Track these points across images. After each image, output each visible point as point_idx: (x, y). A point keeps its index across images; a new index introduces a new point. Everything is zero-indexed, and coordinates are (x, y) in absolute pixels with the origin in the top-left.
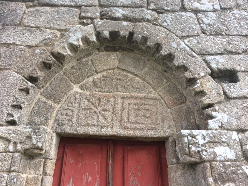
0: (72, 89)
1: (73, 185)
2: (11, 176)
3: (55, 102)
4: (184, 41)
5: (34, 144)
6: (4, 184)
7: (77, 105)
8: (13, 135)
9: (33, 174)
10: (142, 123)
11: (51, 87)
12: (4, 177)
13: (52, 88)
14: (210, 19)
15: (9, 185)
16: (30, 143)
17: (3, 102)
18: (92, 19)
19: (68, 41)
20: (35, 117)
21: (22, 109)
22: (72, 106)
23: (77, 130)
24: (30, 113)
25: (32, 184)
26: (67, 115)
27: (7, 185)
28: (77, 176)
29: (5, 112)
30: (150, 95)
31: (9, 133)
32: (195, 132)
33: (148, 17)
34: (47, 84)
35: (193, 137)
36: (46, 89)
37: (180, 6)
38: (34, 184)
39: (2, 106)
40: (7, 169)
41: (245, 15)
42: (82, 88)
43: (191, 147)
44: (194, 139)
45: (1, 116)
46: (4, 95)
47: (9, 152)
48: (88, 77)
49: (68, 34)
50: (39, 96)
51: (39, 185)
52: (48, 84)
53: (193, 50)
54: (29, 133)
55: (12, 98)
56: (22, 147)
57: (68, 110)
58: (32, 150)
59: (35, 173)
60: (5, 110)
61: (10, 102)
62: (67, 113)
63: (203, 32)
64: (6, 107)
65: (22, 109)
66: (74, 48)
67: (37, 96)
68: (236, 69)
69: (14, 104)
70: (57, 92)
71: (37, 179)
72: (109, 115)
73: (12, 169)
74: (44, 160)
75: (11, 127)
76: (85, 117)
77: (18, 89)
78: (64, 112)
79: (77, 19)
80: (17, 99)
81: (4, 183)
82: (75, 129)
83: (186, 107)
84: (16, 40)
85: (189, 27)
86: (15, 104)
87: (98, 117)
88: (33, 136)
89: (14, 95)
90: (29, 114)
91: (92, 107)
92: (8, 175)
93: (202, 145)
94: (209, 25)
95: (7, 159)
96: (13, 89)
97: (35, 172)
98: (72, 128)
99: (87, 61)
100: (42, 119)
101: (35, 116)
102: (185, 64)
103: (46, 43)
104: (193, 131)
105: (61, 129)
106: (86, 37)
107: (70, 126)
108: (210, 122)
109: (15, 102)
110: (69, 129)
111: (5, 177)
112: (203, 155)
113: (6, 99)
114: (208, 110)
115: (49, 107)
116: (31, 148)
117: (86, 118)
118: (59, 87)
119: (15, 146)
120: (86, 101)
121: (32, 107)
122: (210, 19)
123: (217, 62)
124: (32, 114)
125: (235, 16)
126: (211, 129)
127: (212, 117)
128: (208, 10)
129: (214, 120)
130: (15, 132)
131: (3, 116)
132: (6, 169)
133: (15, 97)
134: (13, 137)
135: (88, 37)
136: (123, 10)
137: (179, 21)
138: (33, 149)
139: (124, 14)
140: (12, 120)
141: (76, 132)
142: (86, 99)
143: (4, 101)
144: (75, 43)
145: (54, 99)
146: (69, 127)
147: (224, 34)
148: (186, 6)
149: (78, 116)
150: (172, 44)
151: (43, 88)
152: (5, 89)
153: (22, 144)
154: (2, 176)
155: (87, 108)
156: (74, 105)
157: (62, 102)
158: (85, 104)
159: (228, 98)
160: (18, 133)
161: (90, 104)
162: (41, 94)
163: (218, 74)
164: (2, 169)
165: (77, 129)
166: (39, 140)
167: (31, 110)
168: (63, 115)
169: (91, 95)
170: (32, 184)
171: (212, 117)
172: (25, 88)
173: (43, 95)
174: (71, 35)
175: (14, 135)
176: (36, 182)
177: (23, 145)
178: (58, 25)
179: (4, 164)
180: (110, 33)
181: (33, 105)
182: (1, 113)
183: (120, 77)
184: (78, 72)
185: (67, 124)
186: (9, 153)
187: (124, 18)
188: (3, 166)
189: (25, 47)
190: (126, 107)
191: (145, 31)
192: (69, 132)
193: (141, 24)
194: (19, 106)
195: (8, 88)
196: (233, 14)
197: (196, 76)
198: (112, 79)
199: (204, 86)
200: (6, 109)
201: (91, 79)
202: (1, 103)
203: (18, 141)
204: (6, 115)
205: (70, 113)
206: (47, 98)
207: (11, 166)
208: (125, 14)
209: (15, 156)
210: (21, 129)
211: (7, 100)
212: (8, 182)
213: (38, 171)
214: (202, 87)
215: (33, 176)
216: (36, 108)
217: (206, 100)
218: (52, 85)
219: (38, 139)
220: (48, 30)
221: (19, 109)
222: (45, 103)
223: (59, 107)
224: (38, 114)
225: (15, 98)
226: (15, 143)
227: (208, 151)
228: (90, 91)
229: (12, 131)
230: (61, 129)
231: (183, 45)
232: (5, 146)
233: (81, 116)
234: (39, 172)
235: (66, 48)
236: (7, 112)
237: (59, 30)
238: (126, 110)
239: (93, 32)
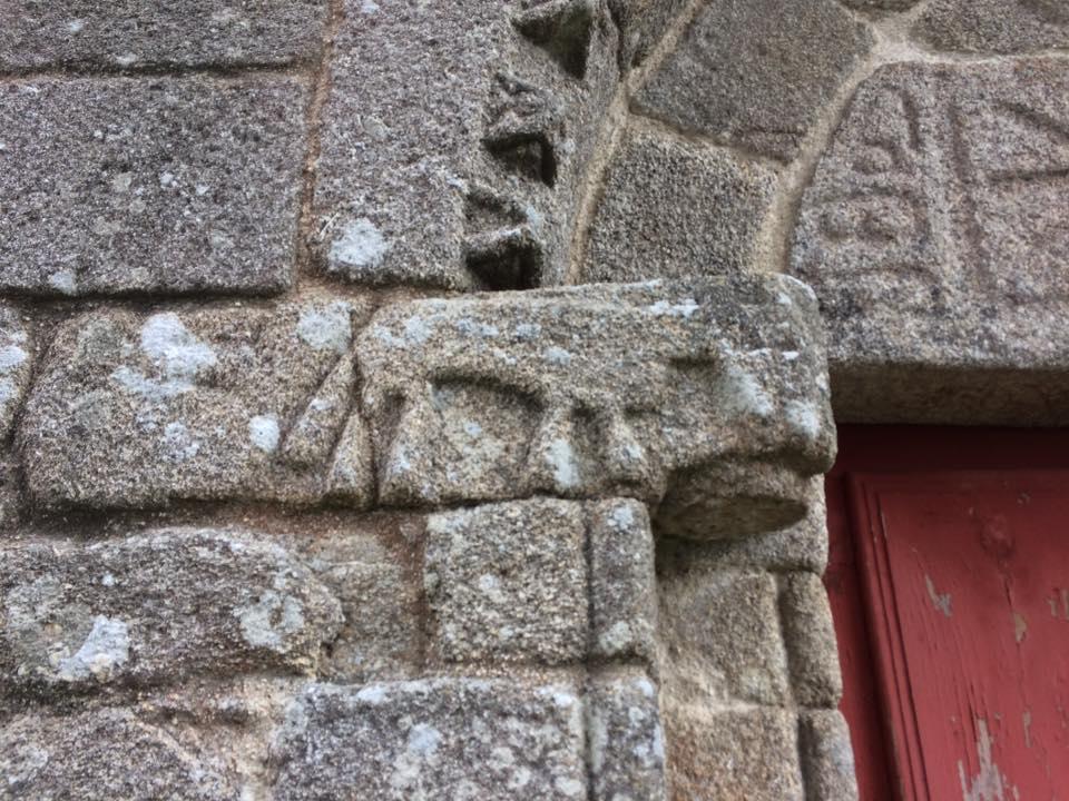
0: (865, 52)
1: (1007, 793)
2: (620, 704)
3: (752, 152)
5: (755, 416)
6: (573, 787)
7: (935, 153)
8: (556, 352)
9: (712, 692)
11: (698, 50)
12: (554, 714)
13: (706, 63)
15: (627, 788)
16: (710, 407)
17: (416, 122)
20: (627, 264)
21: (550, 184)
22: (898, 164)
23: (992, 337)
24: (578, 237)
25: (730, 785)
26: (873, 231)
27: (600, 787)
28: (1027, 719)
29: (452, 186)
31: (520, 339)
34: (664, 42)
36: (666, 68)
38: (745, 778)
39: (417, 150)
40: (566, 636)
45: (427, 215)
46: (417, 67)
47: (548, 490)
50: (623, 124)
51: (796, 790)
52: (670, 38)
54: (683, 326)
55: (485, 84)
56: (650, 450)
57: (876, 198)
58: (742, 471)
59: (734, 689)
60: (442, 172)
61: (474, 111)
62: (869, 217)
64: (452, 149)
65: (550, 184)
67: (609, 127)
69: (500, 125)
70: (753, 77)
71: (766, 741)
73: (617, 636)
74: (773, 584)
76: (1036, 235)
77: (514, 23)
78: (847, 214)
80: (520, 89)
81: (570, 776)
82: (971, 332)
86: (513, 130)
88: (729, 351)
89: (489, 67)
90: (579, 245)
92: (582, 692)
95: (549, 555)
96: (478, 23)
97: (732, 678)
98: (945, 327)
100: (687, 271)
101: (626, 253)
105: (852, 335)
107: (918, 311)
109: (512, 115)
110: (923, 334)
111: (568, 709)
113: (439, 96)
115: (717, 191)
116: (731, 455)
117: (1038, 240)
118: (759, 46)
119: (587, 443)
120: (1002, 120)
121: (589, 197)
124: (601, 246)
130: (563, 331)
131: (437, 219)
132: (557, 638)
133: (501, 79)
134: (560, 368)
140: (511, 246)
141: (992, 349)
142: (1001, 105)
143: (424, 114)
145: (737, 133)
146: (911, 323)
149: (968, 233)
151: (638, 70)
153: (642, 423)
154: (540, 710)
155: (1028, 164)
157: (802, 147)
160: (595, 330)
162: (634, 108)
164: (524, 644)
165: (986, 330)
166: (793, 379)
167: (583, 222)
168: (846, 235)
169: (1031, 73)
170: (730, 785)
172: (561, 14)
173: (650, 115)
175: (565, 352)
176: (762, 762)
177: (660, 432)
179: (530, 591)
181: (590, 187)
182: (423, 195)
185: (894, 298)
186: (550, 502)
188: (519, 612)
192: (930, 352)
194: (536, 151)
195: (438, 23)
200: (453, 162)
202: (406, 126)
203: (609, 395)
204: (459, 212)
205: (899, 218)
206: (681, 132)
207: (591, 612)
209: (611, 523)
210: (610, 306)
211: (450, 104)
212: (607, 766)
213: (755, 672)
215: (722, 708)
216: (624, 204)
218: (703, 43)
219: (779, 372)
221: (536, 180)
222: (678, 166)
223: (792, 183)
224: (646, 244)
225: (506, 89)
226: (585, 415)
228: (1015, 50)
229: (535, 319)
230: (852, 335)
232: (499, 442)
233: (996, 227)
234: (767, 680)
236: (466, 191)
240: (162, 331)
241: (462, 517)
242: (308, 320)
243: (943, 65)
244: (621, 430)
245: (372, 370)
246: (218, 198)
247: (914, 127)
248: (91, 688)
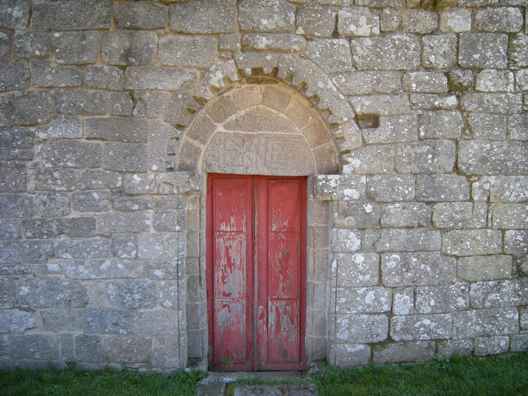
4: (331, 80)
8: (175, 181)
14: (365, 48)
18: (233, 52)
30: (294, 133)
32: (329, 177)
33: (296, 47)
35: (328, 180)
37: (333, 30)
41: (406, 41)
42: (225, 127)
48: (231, 115)
63: (355, 65)
66: (215, 89)
68: (380, 113)
72: (253, 156)
79: (216, 52)
83: (328, 147)
85: (339, 61)
93: (334, 188)
94: (363, 57)
99: (229, 97)
103: (186, 85)
104: (328, 176)
106: (228, 77)
114: (345, 155)
117: (231, 158)
122: (365, 48)
123: (363, 105)
125: (394, 44)
127: (347, 163)
128: (365, 35)
129: (348, 165)
135: (230, 76)
136: (268, 39)
137: (330, 52)
139: (267, 45)
144: (217, 85)
147: (377, 69)
148: (340, 31)
158: (229, 144)
159: (365, 144)
163: (361, 116)
171: (347, 163)
174: (211, 75)
178: (197, 62)
189: (167, 93)
193: (286, 57)
196: (392, 40)
197: (339, 122)
208: (269, 43)
216: (185, 150)
217: (345, 147)
220: (187, 69)
223: (205, 148)
231: (330, 85)
235: (208, 91)
237: (199, 69)
239: (234, 70)
240: (135, 176)
241: (167, 196)
242: (150, 176)
244: (181, 189)
245: (157, 181)
246: (139, 161)
248: (136, 210)
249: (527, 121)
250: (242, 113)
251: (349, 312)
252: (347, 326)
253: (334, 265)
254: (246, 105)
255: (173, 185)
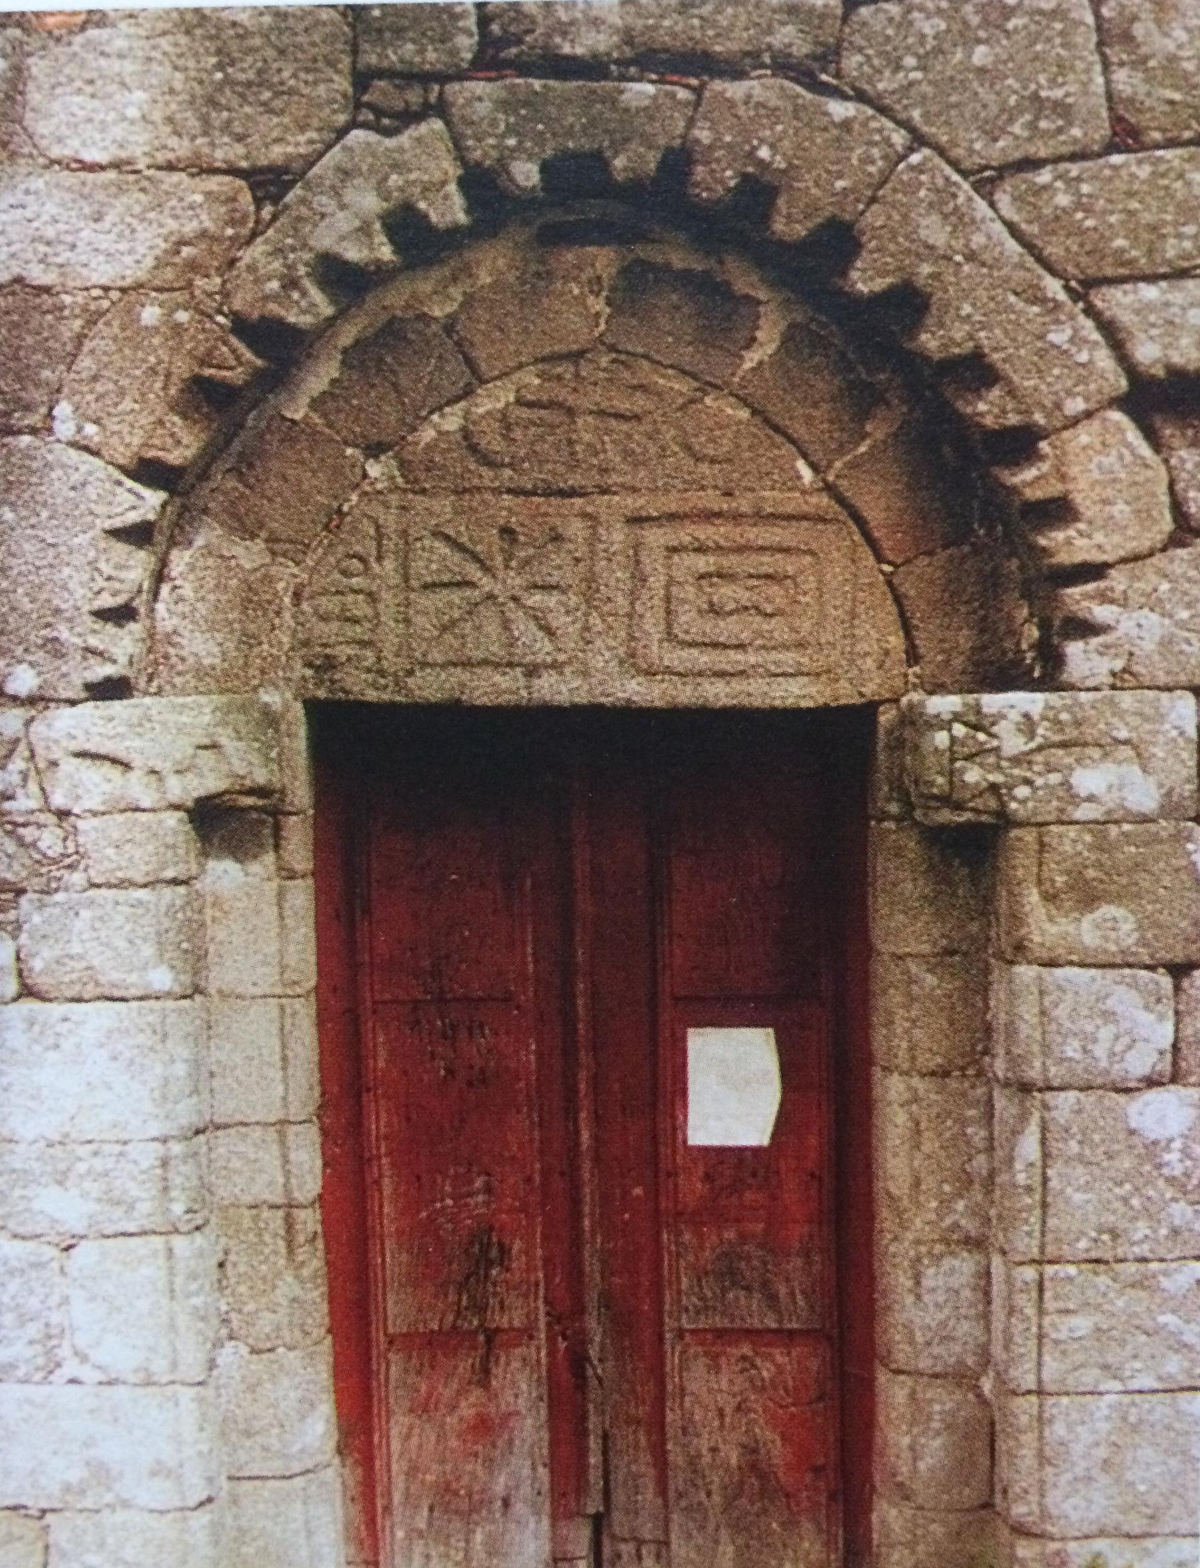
7: (389, 564)
8: (137, 743)
10: (741, 646)
19: (312, 243)
32: (992, 702)
43: (962, 771)
44: (981, 736)
49: (303, 201)
53: (1041, 260)
75: (117, 707)
84: (27, 262)
87: (506, 625)
91: (473, 572)
93: (1016, 760)
102: (987, 351)
106: (408, 208)
108: (1074, 649)
112: (1014, 799)
114: (1075, 591)
120: (437, 544)
126: (1072, 687)
127: (1086, 629)
129: (1095, 641)
138: (240, 793)
142: (437, 534)
144: (353, 253)
150: (924, 222)
152: (41, 533)
156: (375, 565)
161: (457, 557)
171: (1086, 629)
180: (545, 168)
183: (615, 402)
184: (373, 386)
187: (628, 52)
190: (653, 562)
191: (762, 141)
192: (372, 695)
193: (735, 90)
197: (1039, 418)
198: (571, 412)
199: (1074, 471)
201: (451, 420)
214: (1063, 478)
227: (1039, 782)
233: (420, 620)
238: (657, 582)
243: (400, 1233)
247: (380, 545)
249: (944, 5)
250: (489, 401)
251: (1117, 1386)
252: (1102, 1452)
253: (1029, 1147)
254: (518, 353)
255: (127, 766)
